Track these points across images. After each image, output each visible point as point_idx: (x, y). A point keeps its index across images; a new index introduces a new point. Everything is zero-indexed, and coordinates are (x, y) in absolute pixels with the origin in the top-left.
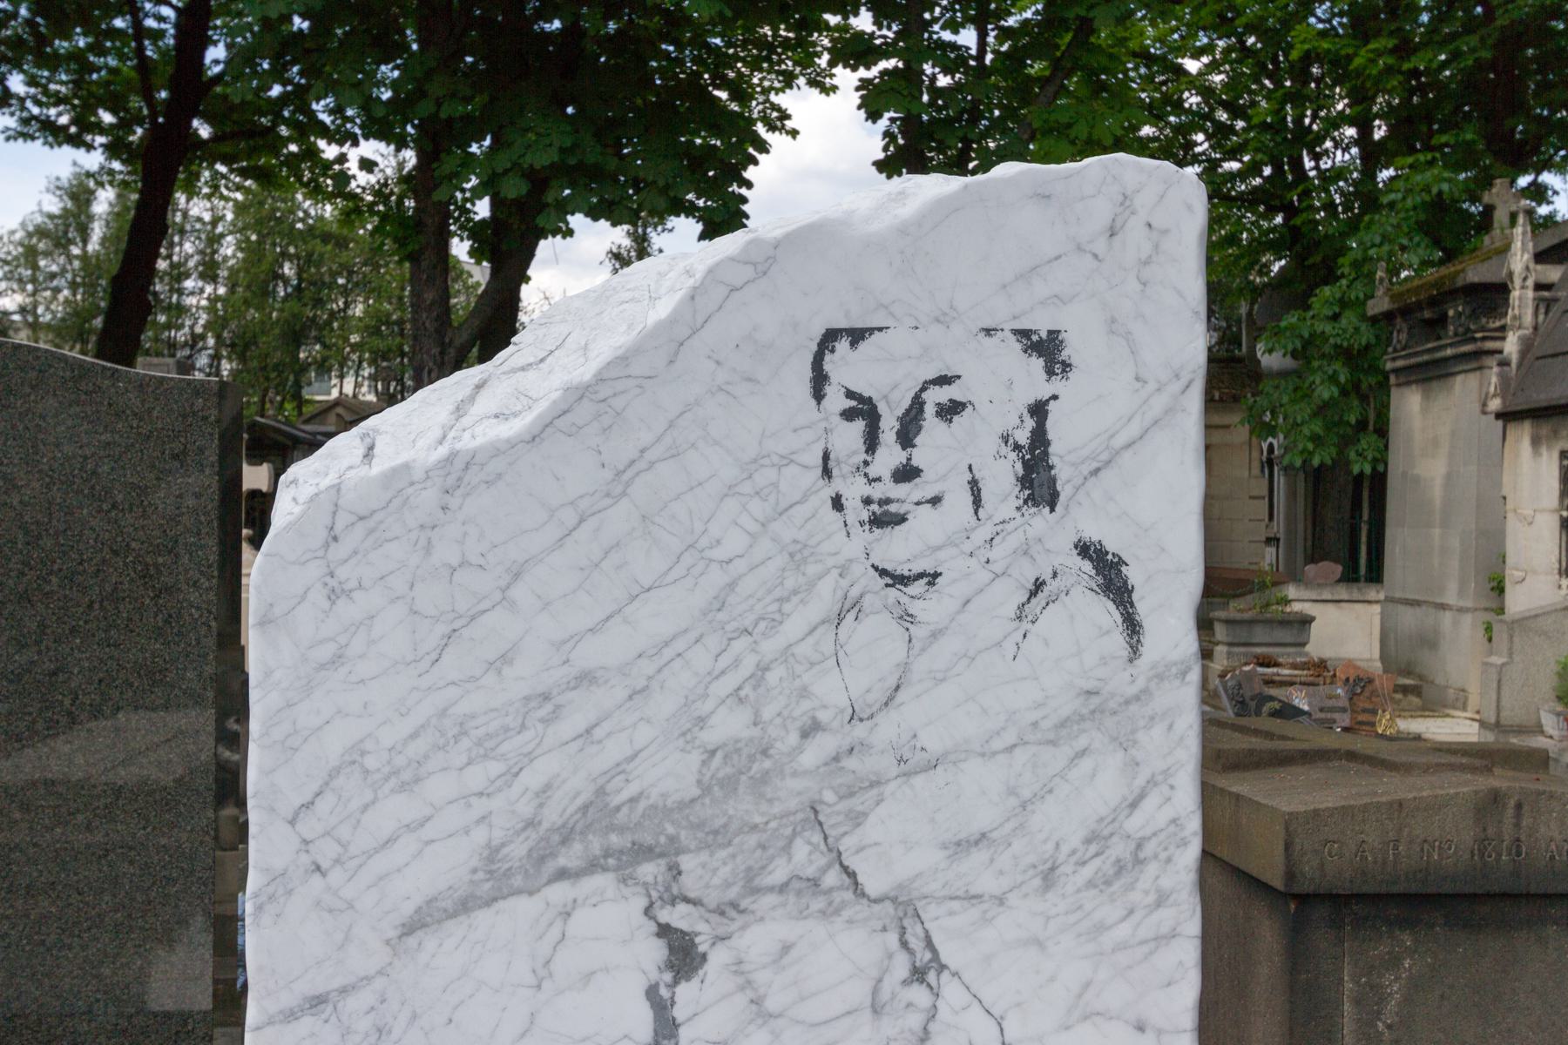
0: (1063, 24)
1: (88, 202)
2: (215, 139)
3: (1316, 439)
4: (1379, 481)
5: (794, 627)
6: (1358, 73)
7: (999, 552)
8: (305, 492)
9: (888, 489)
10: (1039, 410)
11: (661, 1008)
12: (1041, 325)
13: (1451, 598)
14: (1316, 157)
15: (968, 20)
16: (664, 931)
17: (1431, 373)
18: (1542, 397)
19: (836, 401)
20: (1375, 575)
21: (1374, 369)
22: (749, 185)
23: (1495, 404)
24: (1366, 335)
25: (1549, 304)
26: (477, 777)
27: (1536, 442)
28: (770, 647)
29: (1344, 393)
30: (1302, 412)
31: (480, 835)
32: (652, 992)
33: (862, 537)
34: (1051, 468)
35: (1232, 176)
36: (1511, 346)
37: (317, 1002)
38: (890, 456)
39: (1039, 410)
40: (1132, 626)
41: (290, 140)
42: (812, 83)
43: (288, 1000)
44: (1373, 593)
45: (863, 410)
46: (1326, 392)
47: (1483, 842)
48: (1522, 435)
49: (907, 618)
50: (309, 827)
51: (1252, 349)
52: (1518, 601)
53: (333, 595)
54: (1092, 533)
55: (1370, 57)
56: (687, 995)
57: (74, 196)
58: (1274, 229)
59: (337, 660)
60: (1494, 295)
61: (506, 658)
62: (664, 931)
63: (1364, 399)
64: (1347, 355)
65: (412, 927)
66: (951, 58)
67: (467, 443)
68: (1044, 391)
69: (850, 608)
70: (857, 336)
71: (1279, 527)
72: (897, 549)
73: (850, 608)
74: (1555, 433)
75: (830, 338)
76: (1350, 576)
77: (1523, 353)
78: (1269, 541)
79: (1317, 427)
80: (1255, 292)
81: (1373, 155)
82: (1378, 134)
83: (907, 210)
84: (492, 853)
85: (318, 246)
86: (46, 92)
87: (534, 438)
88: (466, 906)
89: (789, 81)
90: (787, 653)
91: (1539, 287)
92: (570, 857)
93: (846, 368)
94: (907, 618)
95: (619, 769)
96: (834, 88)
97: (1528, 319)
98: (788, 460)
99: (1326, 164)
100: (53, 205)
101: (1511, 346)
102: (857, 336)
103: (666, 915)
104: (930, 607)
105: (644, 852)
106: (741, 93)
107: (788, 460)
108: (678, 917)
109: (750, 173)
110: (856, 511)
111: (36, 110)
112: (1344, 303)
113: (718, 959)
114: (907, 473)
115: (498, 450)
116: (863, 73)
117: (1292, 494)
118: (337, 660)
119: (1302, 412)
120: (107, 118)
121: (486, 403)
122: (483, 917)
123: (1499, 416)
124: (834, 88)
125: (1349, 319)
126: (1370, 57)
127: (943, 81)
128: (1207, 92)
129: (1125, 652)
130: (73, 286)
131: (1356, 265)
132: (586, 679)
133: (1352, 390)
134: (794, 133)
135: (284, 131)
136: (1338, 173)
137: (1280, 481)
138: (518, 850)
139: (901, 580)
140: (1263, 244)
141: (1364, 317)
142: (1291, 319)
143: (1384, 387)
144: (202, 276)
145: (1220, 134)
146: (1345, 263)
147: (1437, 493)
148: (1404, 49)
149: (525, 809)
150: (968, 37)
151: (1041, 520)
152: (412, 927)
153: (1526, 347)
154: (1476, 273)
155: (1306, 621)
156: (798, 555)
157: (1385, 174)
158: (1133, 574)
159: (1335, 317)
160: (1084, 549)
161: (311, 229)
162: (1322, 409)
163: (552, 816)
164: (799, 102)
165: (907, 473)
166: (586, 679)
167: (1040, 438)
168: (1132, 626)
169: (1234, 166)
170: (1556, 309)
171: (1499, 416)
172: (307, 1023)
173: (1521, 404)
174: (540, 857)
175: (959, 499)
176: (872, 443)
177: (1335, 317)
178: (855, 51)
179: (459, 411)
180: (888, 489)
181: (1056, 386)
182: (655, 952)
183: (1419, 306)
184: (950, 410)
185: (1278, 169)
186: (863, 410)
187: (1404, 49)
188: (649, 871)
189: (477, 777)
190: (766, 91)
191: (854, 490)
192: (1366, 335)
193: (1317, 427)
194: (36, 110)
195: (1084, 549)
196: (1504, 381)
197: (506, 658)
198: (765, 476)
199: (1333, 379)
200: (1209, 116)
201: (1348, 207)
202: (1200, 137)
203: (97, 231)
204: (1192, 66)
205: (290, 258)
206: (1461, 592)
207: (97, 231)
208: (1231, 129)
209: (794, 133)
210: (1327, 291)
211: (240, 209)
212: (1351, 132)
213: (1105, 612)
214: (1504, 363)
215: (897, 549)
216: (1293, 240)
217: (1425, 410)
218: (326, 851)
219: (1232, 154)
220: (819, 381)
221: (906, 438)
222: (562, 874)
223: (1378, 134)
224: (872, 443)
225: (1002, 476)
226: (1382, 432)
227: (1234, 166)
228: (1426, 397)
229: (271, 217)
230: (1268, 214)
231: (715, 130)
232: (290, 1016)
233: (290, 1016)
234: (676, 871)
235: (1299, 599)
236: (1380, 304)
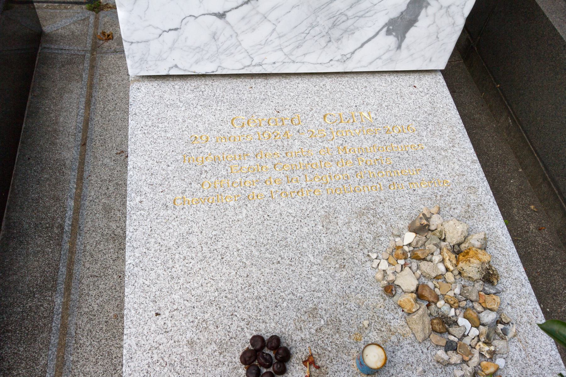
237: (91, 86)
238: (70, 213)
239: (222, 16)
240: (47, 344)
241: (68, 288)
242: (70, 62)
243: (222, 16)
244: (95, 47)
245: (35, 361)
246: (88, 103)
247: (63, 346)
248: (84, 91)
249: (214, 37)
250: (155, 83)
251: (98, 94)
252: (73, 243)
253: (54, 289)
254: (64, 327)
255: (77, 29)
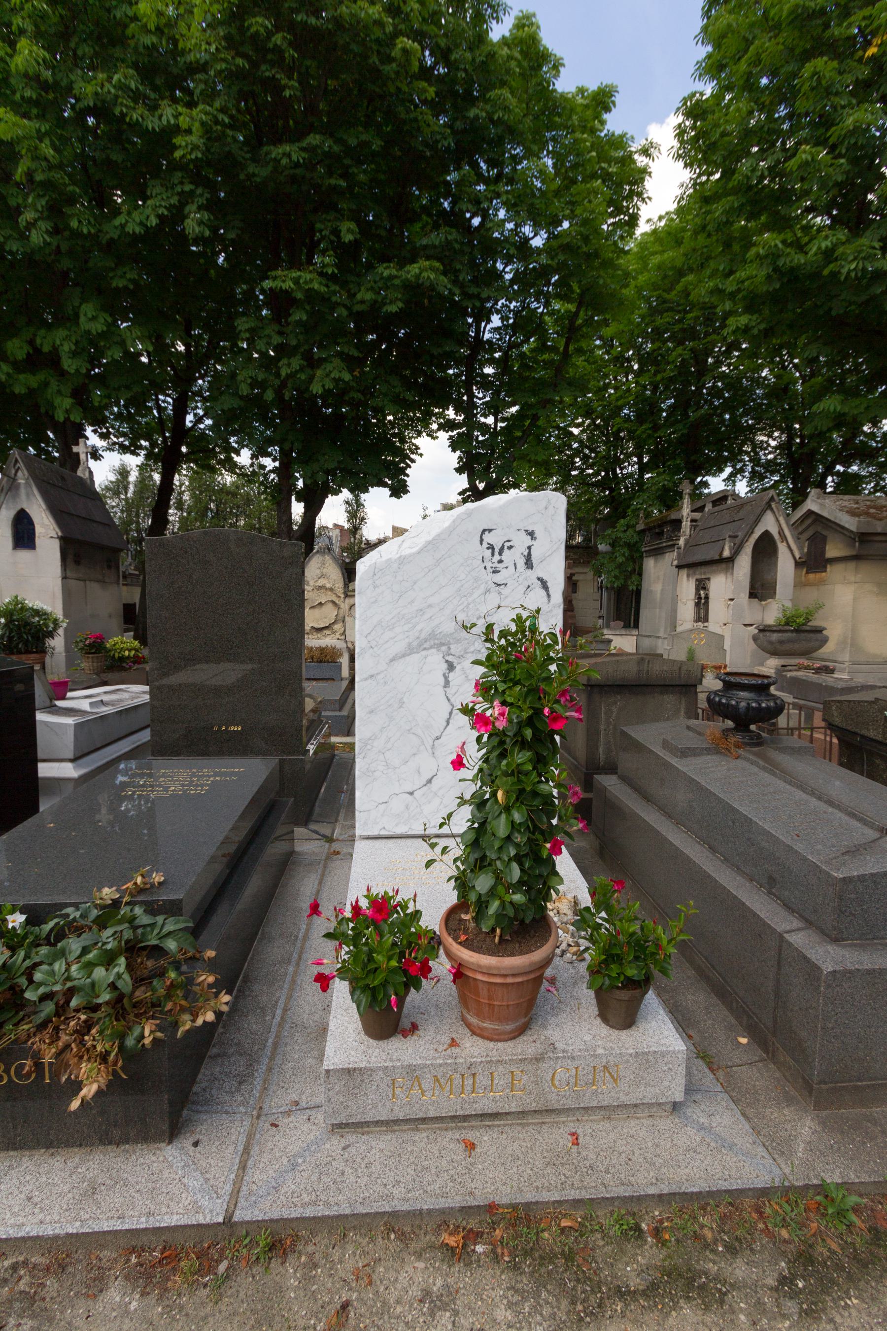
0: (527, 417)
1: (127, 477)
2: (188, 454)
3: (616, 577)
4: (638, 593)
5: (475, 595)
6: (639, 437)
7: (520, 579)
8: (368, 564)
9: (496, 565)
10: (529, 548)
11: (446, 678)
12: (530, 529)
13: (661, 634)
14: (621, 469)
15: (490, 413)
16: (447, 661)
17: (658, 552)
18: (691, 560)
19: (485, 545)
20: (636, 626)
21: (638, 551)
22: (408, 476)
23: (675, 563)
24: (636, 538)
25: (695, 527)
26: (406, 628)
27: (688, 576)
28: (470, 600)
29: (627, 559)
30: (611, 566)
31: (407, 640)
32: (444, 675)
33: (491, 575)
34: (686, 166)
35: (589, 475)
36: (681, 542)
37: (372, 676)
38: (497, 557)
39: (529, 548)
40: (549, 596)
41: (220, 453)
42: (428, 435)
43: (365, 676)
44: (635, 632)
45: (491, 547)
46: (620, 559)
47: (639, 672)
48: (684, 573)
49: (500, 593)
50: (369, 638)
51: (596, 543)
52: (679, 629)
53: (375, 587)
54: (540, 575)
55: (643, 429)
56: (452, 676)
57: (120, 474)
58: (605, 496)
59: (376, 601)
60: (678, 523)
61: (412, 601)
62: (447, 661)
63: (634, 562)
64: (629, 545)
65: (392, 660)
66: (484, 428)
67: (403, 554)
68: (530, 543)
69: (488, 591)
70: (490, 531)
71: (604, 612)
72: (498, 578)
73: (488, 591)
74: (694, 573)
75: (484, 531)
76: (627, 626)
77: (685, 545)
78: (600, 617)
79: (617, 572)
80: (598, 521)
81: (643, 468)
82: (645, 460)
83: (501, 503)
84: (410, 644)
85: (224, 497)
86: (118, 431)
87: (419, 553)
88: (404, 656)
89: (419, 434)
90: (474, 601)
91: (692, 521)
92: (426, 645)
93: (488, 538)
94: (500, 593)
95: (437, 626)
96: (437, 437)
97: (688, 532)
98: (474, 558)
99: (625, 472)
100: (113, 477)
101: (681, 542)
102: (490, 531)
103: (447, 658)
104: (505, 591)
105: (443, 644)
106: (403, 441)
107: (474, 558)
108: (450, 658)
109: (408, 471)
110: (489, 570)
111: (115, 440)
112: (628, 526)
113: (458, 668)
114: (500, 561)
115: (410, 555)
116: (450, 433)
117: (609, 599)
118: (376, 601)
119: (611, 566)
120: (144, 443)
121: (405, 545)
122: (408, 658)
123: (677, 567)
124: (437, 437)
125: (630, 532)
126: (643, 429)
127: (481, 438)
128: (581, 442)
129: (546, 598)
130: (122, 511)
131: (633, 511)
132: (430, 606)
133: (632, 559)
134: (421, 455)
135: (217, 450)
136: (631, 475)
137: (605, 594)
138: (415, 644)
139: (499, 585)
140: (599, 503)
141: (635, 532)
142: (609, 532)
143: (641, 557)
144: (176, 508)
145: (585, 459)
146: (629, 512)
147: (658, 595)
148: (656, 428)
149: (417, 634)
150: (490, 420)
151: (529, 572)
152: (392, 660)
153: (687, 542)
154: (674, 516)
155: (610, 641)
156: (476, 579)
157: (648, 476)
158: (549, 584)
159: (625, 531)
160: (539, 579)
161: (222, 489)
162: (620, 566)
163: (423, 636)
164: (423, 442)
165: (500, 561)
166: (430, 606)
167: (529, 554)
168: (549, 596)
169: (591, 471)
170: (698, 529)
171: (677, 567)
172: (369, 681)
173: (683, 563)
174: (420, 645)
175: (512, 567)
176: (493, 555)
177: (625, 531)
178: (449, 425)
179: (400, 547)
180: (496, 565)
181: (533, 542)
182: (445, 666)
183: (655, 527)
184: (510, 547)
185: (607, 474)
186: (491, 547)
187: (656, 428)
188: (444, 648)
189: (406, 628)
190: (410, 438)
191: (489, 565)
192: (636, 538)
193: (617, 572)
194: (115, 440)
195: (539, 579)
196: (679, 554)
197: (412, 601)
198: (470, 562)
199: (623, 555)
200: (582, 452)
201: (633, 489)
202: (577, 460)
203: (131, 488)
204: (576, 431)
205: (213, 501)
206: (665, 631)
207: (131, 488)
208: (590, 457)
209: (421, 455)
210: (622, 521)
211: (191, 480)
212: (635, 459)
213: (543, 593)
214: (679, 548)
215: (498, 578)
216: (612, 501)
217: (655, 566)
218: (373, 644)
219: (591, 466)
220: (482, 541)
221: (500, 554)
222: (425, 649)
223: (645, 460)
224: (493, 555)
225: (521, 562)
226: (640, 574)
227: (591, 471)
228: (656, 561)
229: (205, 484)
230: (603, 491)
231: (394, 455)
232: (366, 679)
233: (366, 679)
234: (449, 648)
235: (608, 634)
236: (641, 527)
237: (323, 875)
238: (303, 931)
239: (411, 793)
240: (282, 988)
241: (298, 964)
242: (311, 864)
243: (411, 793)
244: (328, 858)
245: (274, 994)
246: (320, 883)
247: (292, 989)
248: (243, 1139)
249: (407, 807)
250: (370, 841)
251: (328, 879)
252: (303, 944)
253: (289, 963)
254: (293, 981)
255: (316, 850)
